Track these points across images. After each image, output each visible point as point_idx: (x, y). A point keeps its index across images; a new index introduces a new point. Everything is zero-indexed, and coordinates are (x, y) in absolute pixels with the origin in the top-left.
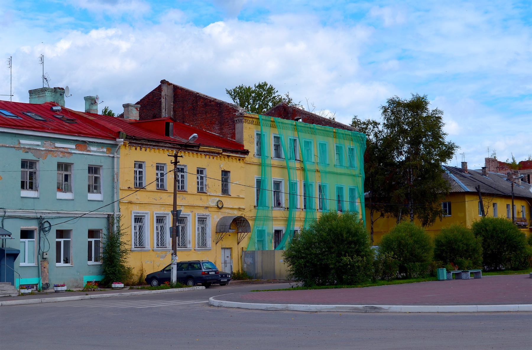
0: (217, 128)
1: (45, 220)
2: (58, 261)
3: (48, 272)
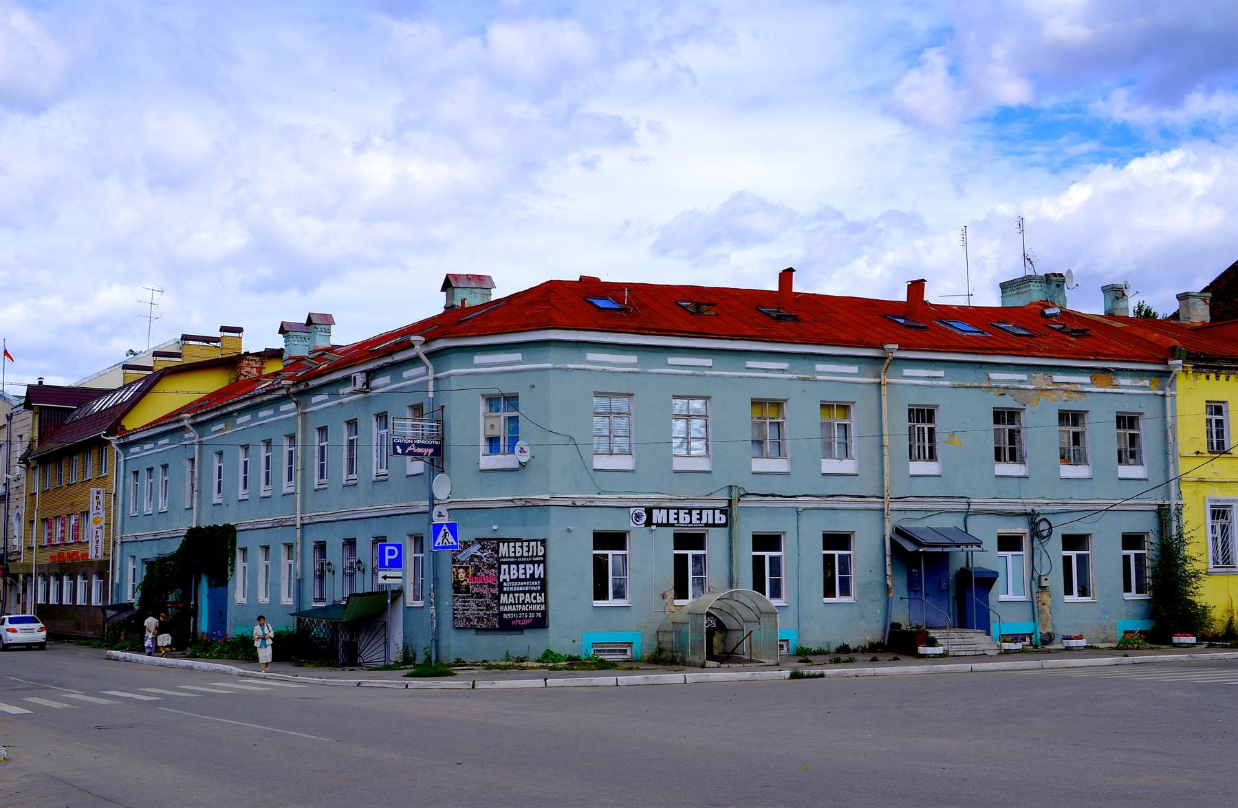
1: (1041, 517)
2: (1068, 591)
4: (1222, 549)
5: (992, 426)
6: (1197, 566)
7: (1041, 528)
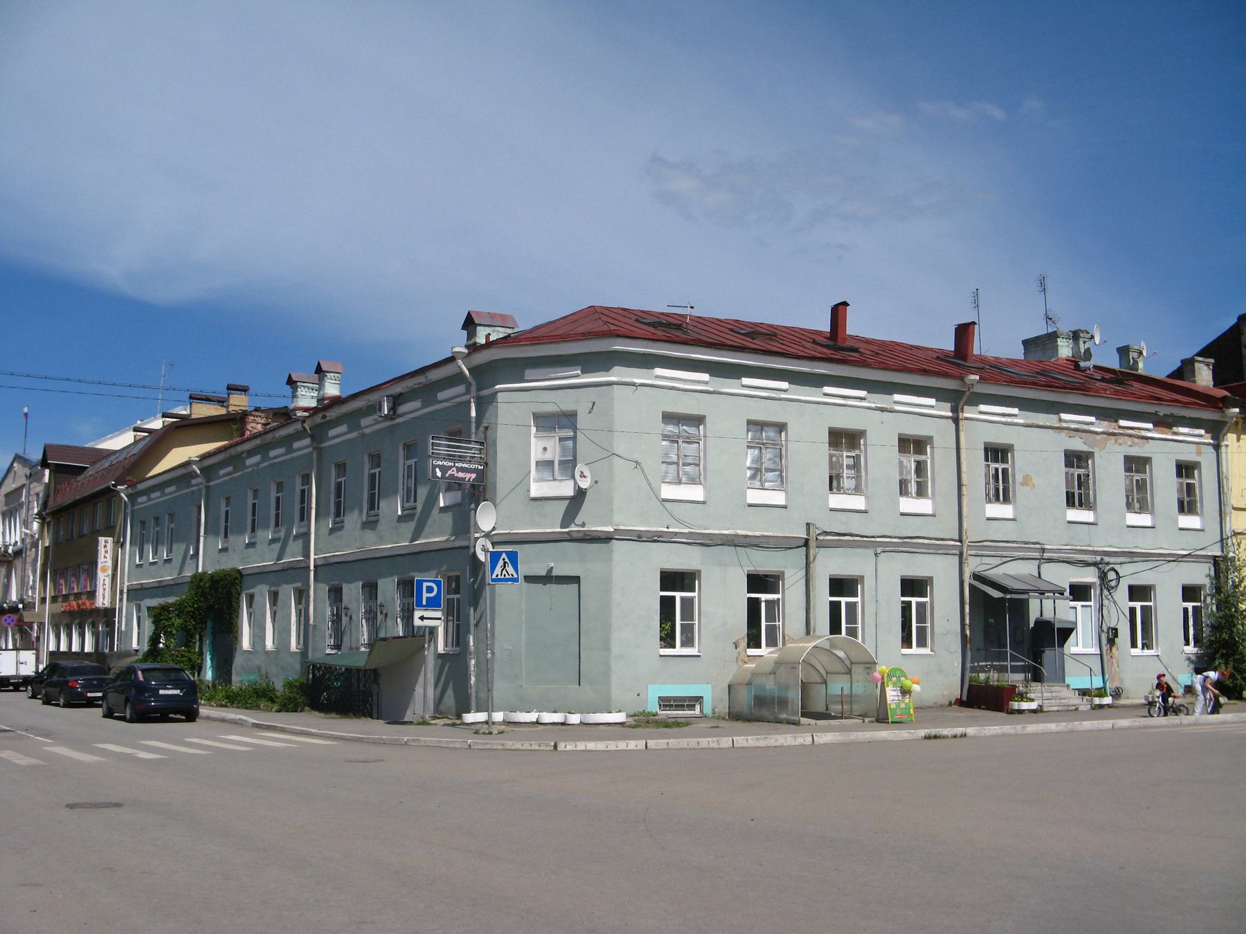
1: (1111, 566)
2: (1134, 645)
3: (1118, 666)
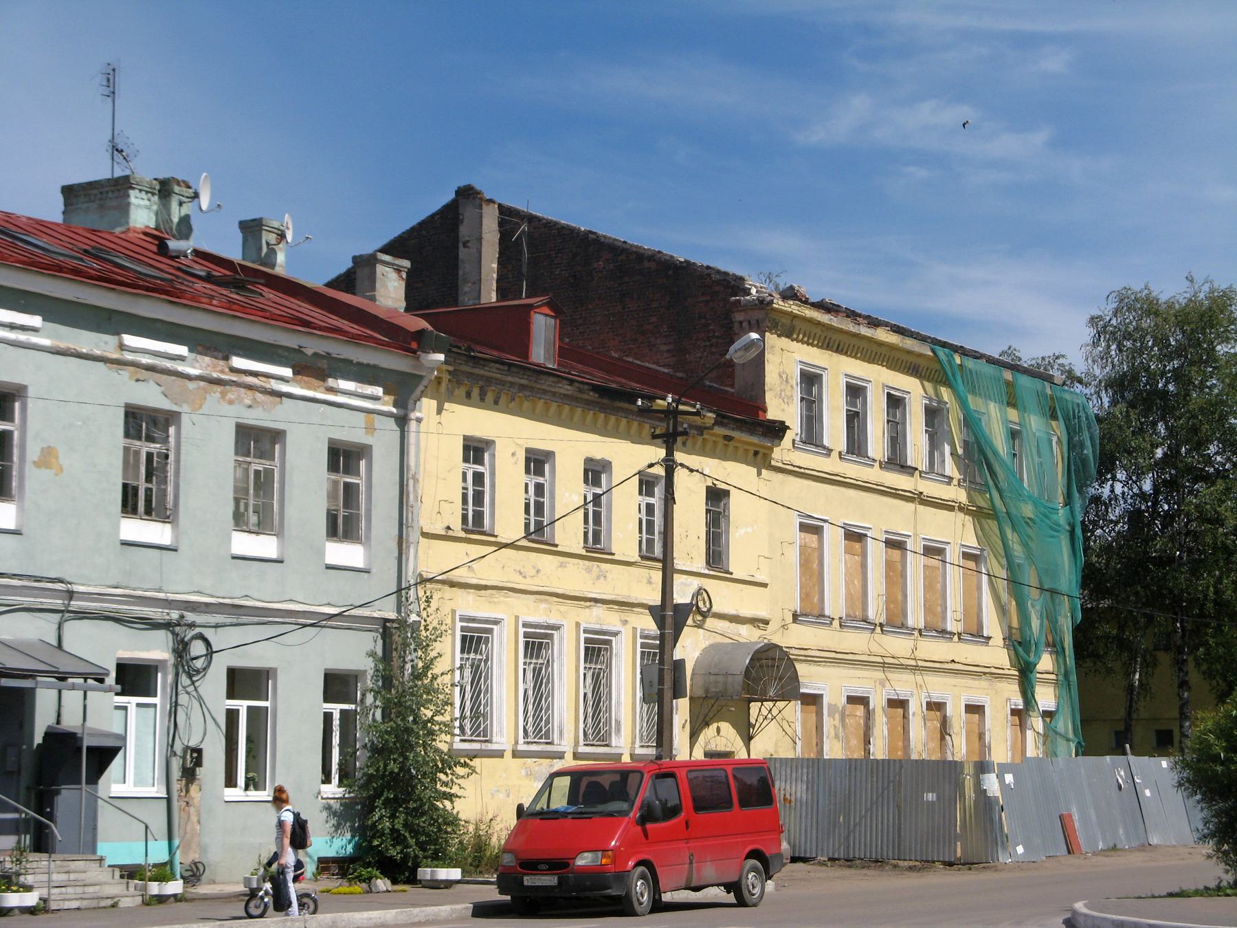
0: (664, 348)
1: (198, 630)
2: (230, 781)
3: (199, 822)
4: (534, 716)
5: (119, 439)
6: (442, 743)
7: (194, 653)
